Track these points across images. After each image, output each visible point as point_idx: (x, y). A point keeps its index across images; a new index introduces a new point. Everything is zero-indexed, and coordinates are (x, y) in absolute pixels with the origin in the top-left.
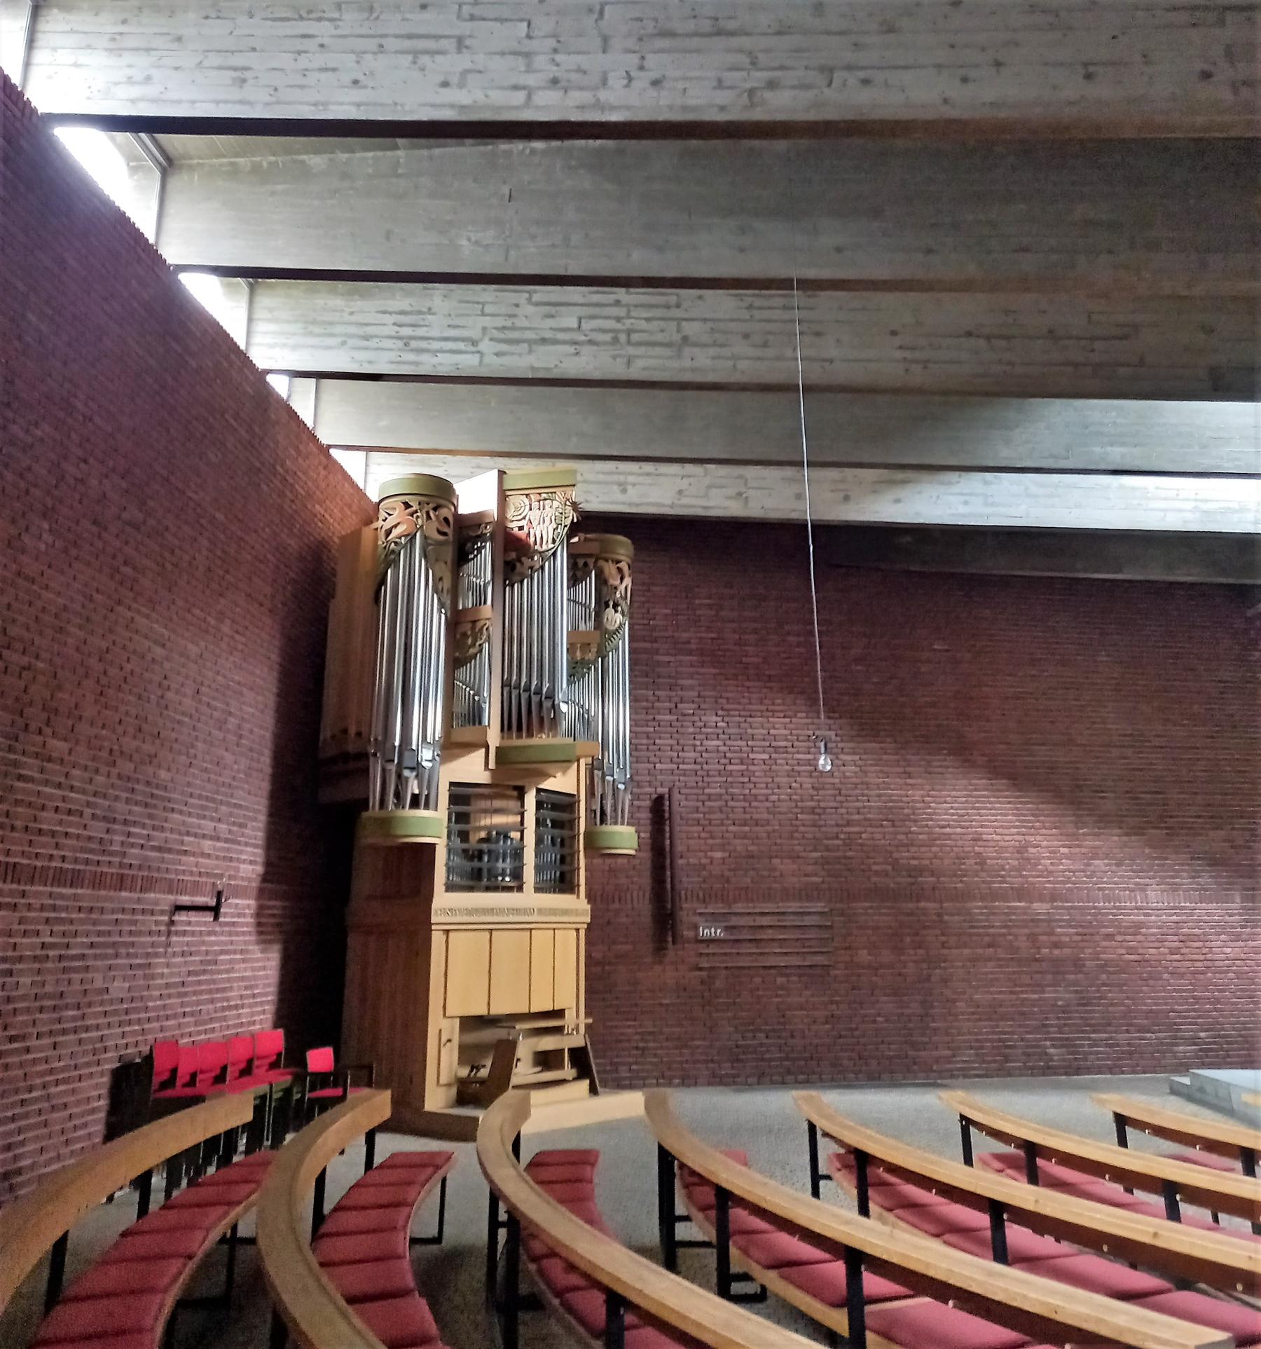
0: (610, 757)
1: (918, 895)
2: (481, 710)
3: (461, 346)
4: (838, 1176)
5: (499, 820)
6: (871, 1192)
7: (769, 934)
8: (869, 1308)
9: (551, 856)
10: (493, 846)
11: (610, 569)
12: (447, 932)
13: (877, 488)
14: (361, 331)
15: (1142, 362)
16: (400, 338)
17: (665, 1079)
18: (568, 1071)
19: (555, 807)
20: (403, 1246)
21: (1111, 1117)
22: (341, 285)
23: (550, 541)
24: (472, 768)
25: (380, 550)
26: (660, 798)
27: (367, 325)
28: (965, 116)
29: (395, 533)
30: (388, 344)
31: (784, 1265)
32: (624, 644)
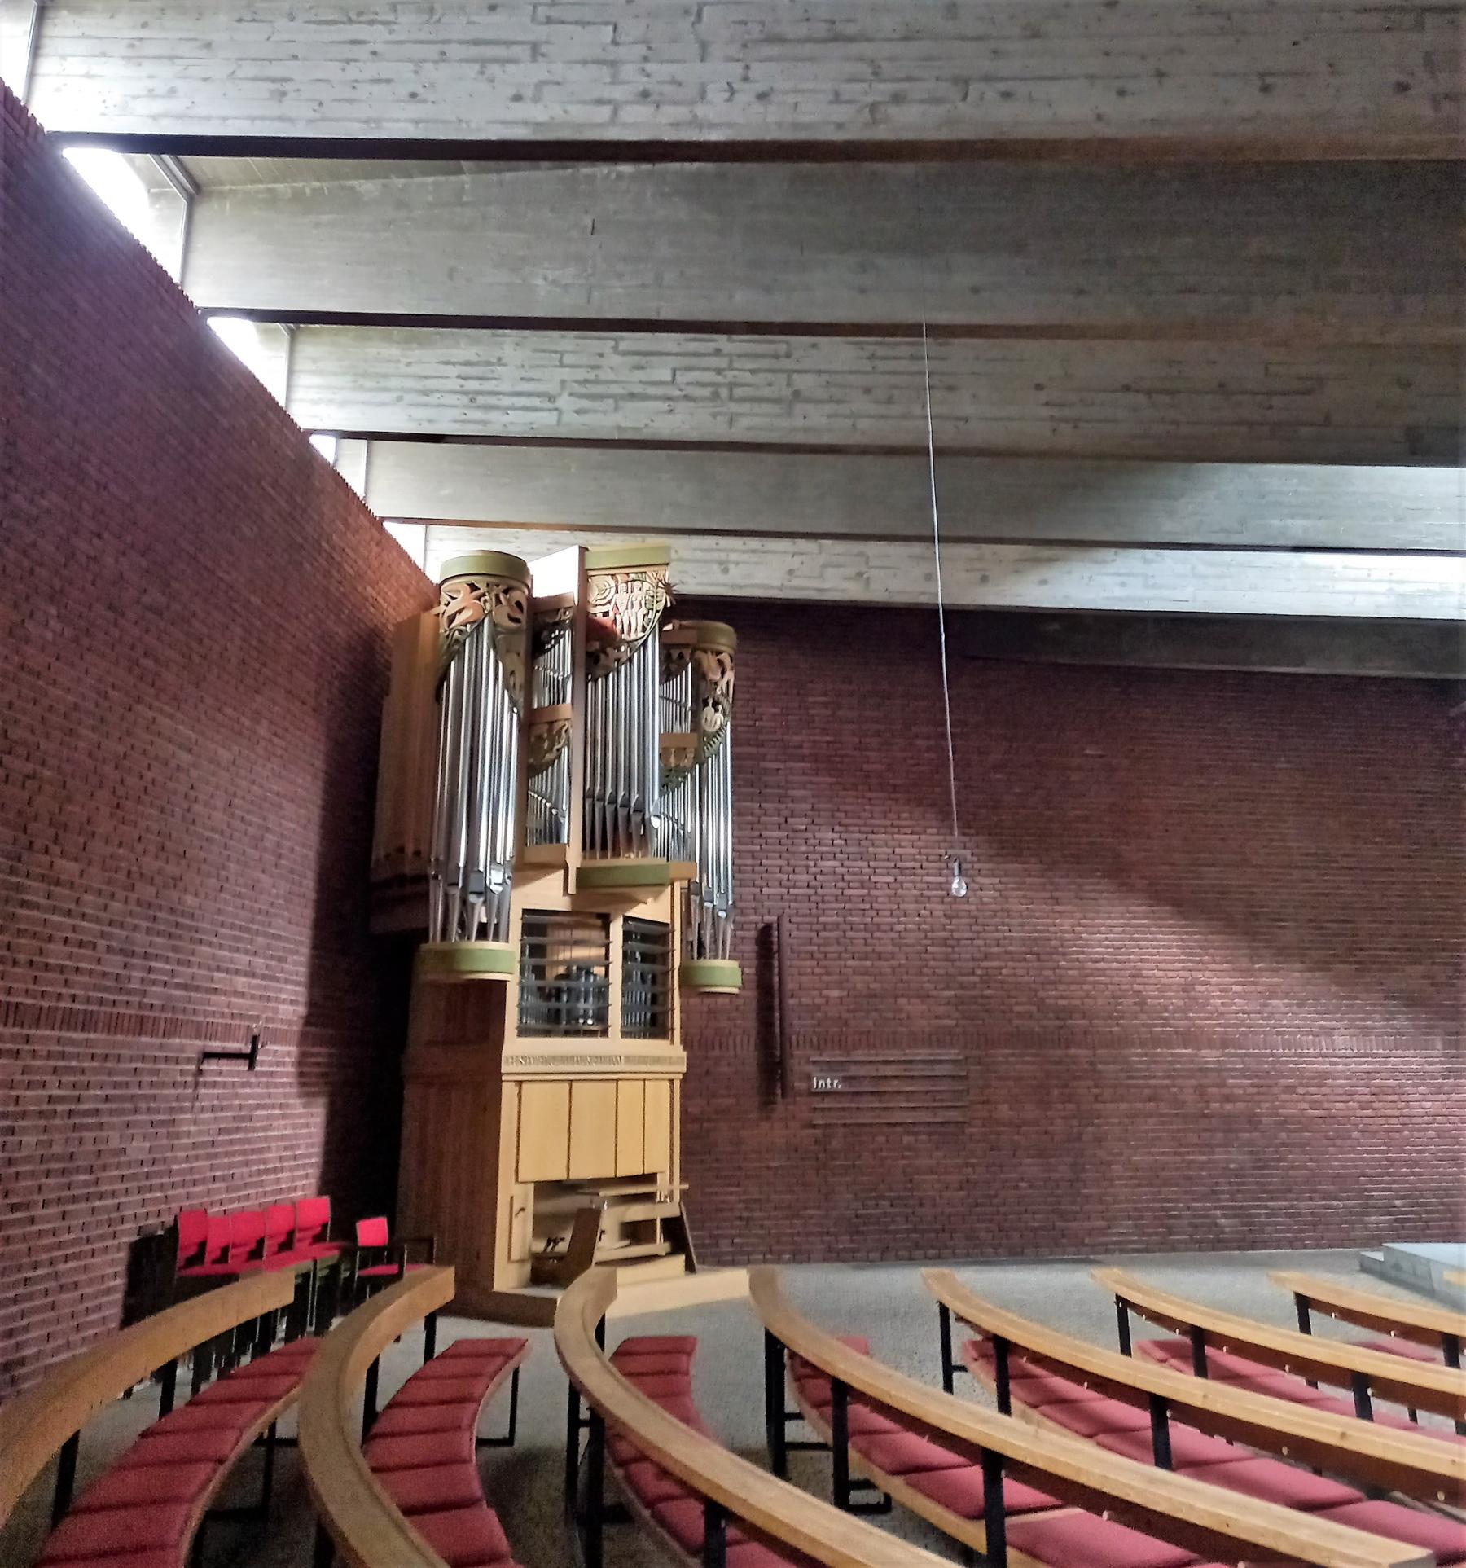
0: (709, 880)
1: (1068, 1040)
2: (559, 825)
3: (536, 402)
4: (974, 1366)
5: (580, 953)
6: (1012, 1386)
7: (894, 1086)
8: (1010, 1521)
9: (641, 995)
10: (573, 984)
11: (709, 662)
12: (520, 1083)
13: (1019, 567)
14: (419, 385)
15: (1327, 421)
16: (465, 393)
17: (773, 1254)
18: (660, 1245)
19: (645, 938)
20: (469, 1448)
21: (1292, 1298)
22: (396, 331)
23: (640, 628)
24: (549, 893)
25: (442, 639)
26: (767, 928)
27: (426, 377)
28: (1122, 135)
29: (459, 619)
30: (451, 399)
31: (911, 1470)
32: (725, 748)
